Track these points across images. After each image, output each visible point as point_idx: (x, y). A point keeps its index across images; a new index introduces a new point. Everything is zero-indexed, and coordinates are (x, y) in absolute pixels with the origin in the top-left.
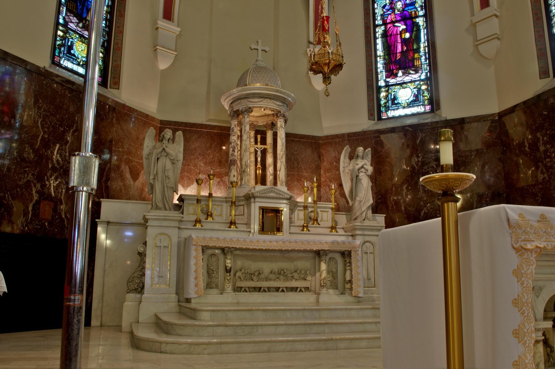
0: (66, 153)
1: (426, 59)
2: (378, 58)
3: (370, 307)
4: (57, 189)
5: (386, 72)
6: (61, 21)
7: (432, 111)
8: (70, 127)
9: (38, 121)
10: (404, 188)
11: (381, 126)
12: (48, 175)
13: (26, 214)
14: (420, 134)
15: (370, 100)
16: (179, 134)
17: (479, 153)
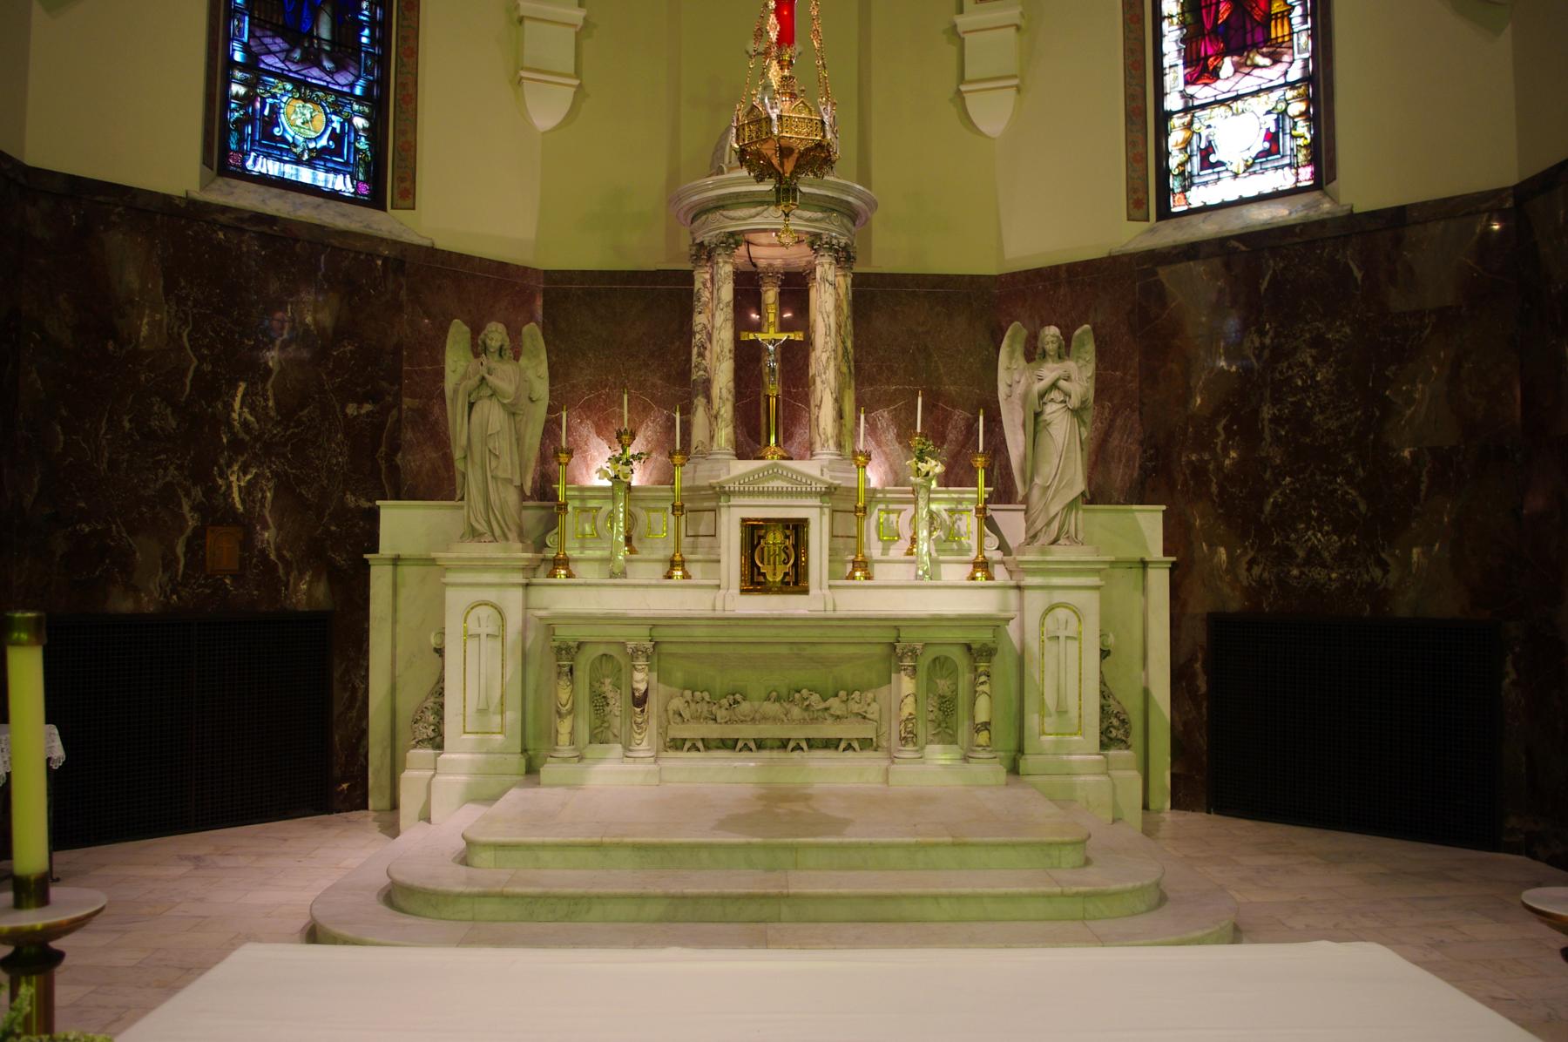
0: (266, 400)
1: (1304, 16)
2: (1165, 24)
3: (949, 839)
4: (249, 493)
5: (1186, 65)
7: (1319, 182)
9: (180, 335)
10: (1220, 428)
11: (1169, 236)
12: (222, 461)
13: (169, 563)
14: (1271, 263)
15: (1135, 159)
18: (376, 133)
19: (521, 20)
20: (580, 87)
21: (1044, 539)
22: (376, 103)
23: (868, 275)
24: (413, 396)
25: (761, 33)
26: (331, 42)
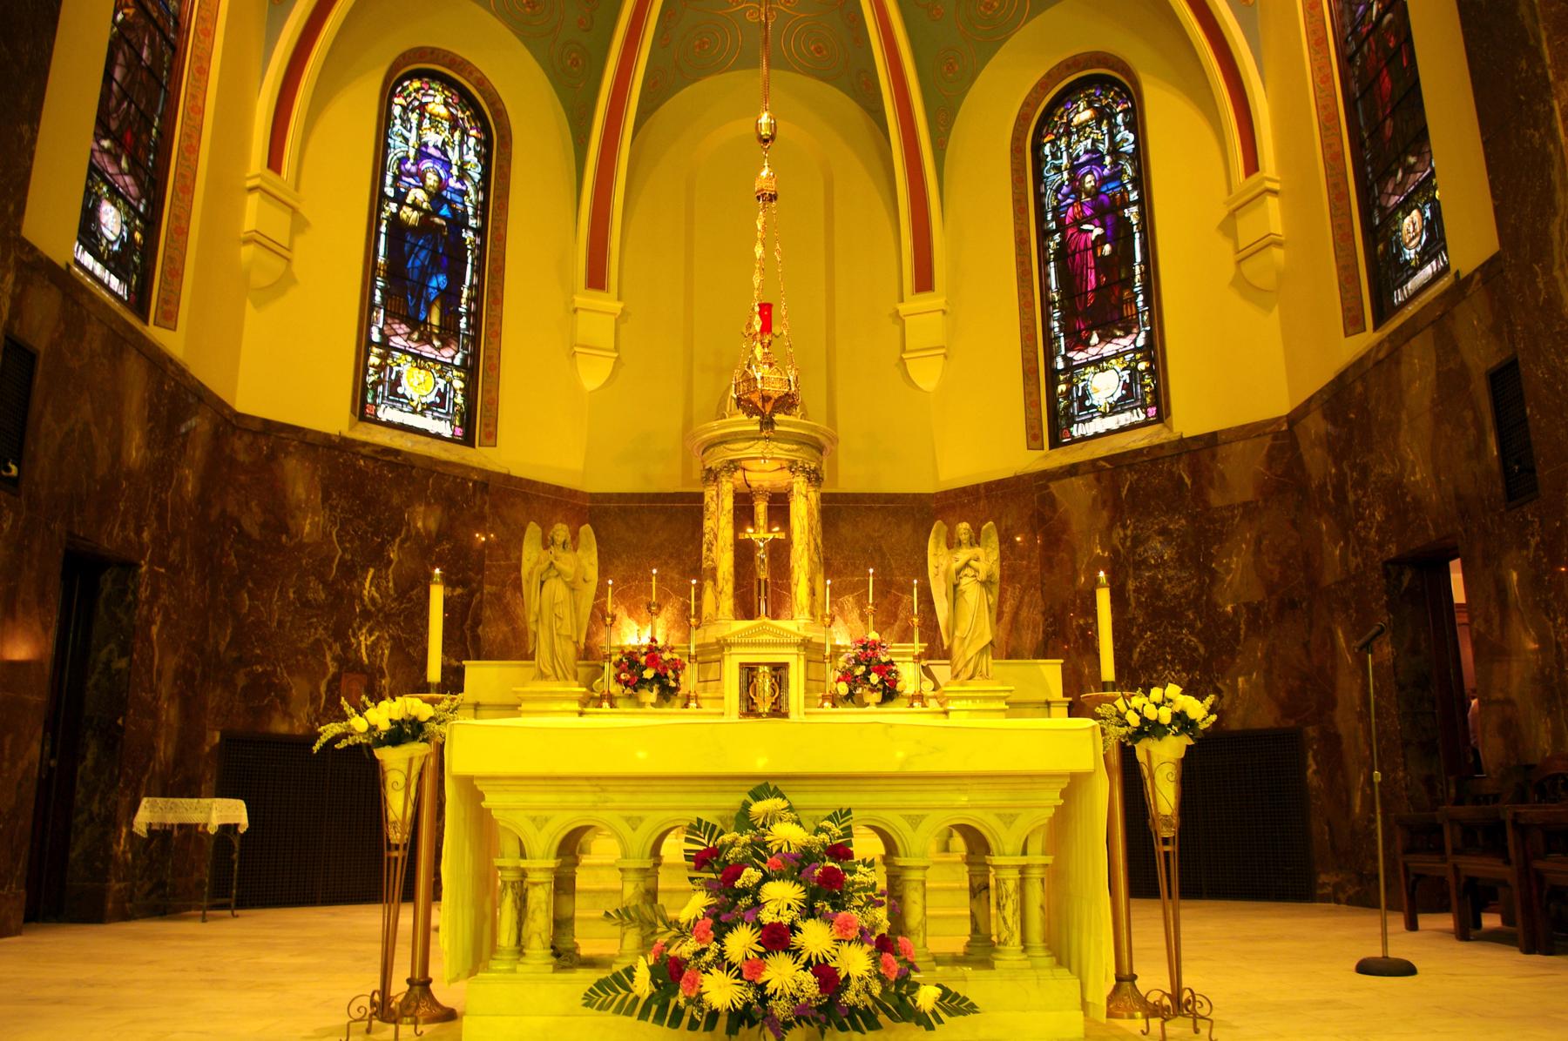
6: (376, 337)
8: (394, 534)
13: (314, 699)
16: (586, 530)
17: (1249, 510)
18: (469, 393)
19: (575, 311)
20: (618, 358)
21: (963, 676)
22: (470, 370)
23: (834, 495)
24: (492, 584)
25: (750, 325)
26: (440, 327)
